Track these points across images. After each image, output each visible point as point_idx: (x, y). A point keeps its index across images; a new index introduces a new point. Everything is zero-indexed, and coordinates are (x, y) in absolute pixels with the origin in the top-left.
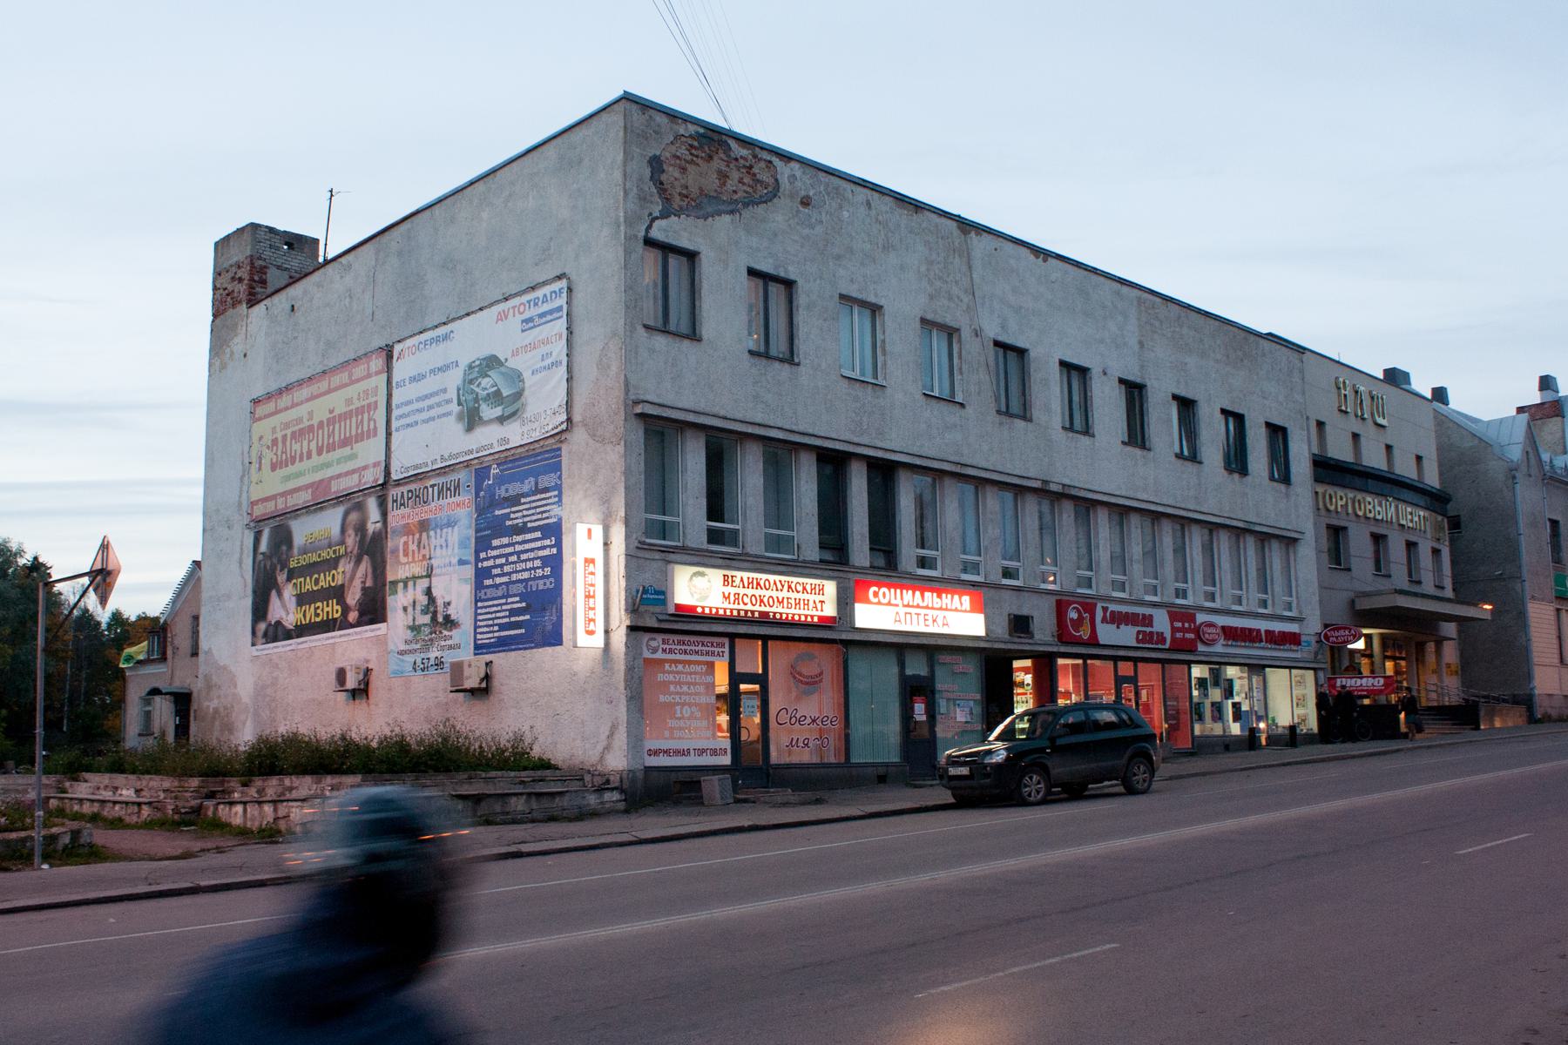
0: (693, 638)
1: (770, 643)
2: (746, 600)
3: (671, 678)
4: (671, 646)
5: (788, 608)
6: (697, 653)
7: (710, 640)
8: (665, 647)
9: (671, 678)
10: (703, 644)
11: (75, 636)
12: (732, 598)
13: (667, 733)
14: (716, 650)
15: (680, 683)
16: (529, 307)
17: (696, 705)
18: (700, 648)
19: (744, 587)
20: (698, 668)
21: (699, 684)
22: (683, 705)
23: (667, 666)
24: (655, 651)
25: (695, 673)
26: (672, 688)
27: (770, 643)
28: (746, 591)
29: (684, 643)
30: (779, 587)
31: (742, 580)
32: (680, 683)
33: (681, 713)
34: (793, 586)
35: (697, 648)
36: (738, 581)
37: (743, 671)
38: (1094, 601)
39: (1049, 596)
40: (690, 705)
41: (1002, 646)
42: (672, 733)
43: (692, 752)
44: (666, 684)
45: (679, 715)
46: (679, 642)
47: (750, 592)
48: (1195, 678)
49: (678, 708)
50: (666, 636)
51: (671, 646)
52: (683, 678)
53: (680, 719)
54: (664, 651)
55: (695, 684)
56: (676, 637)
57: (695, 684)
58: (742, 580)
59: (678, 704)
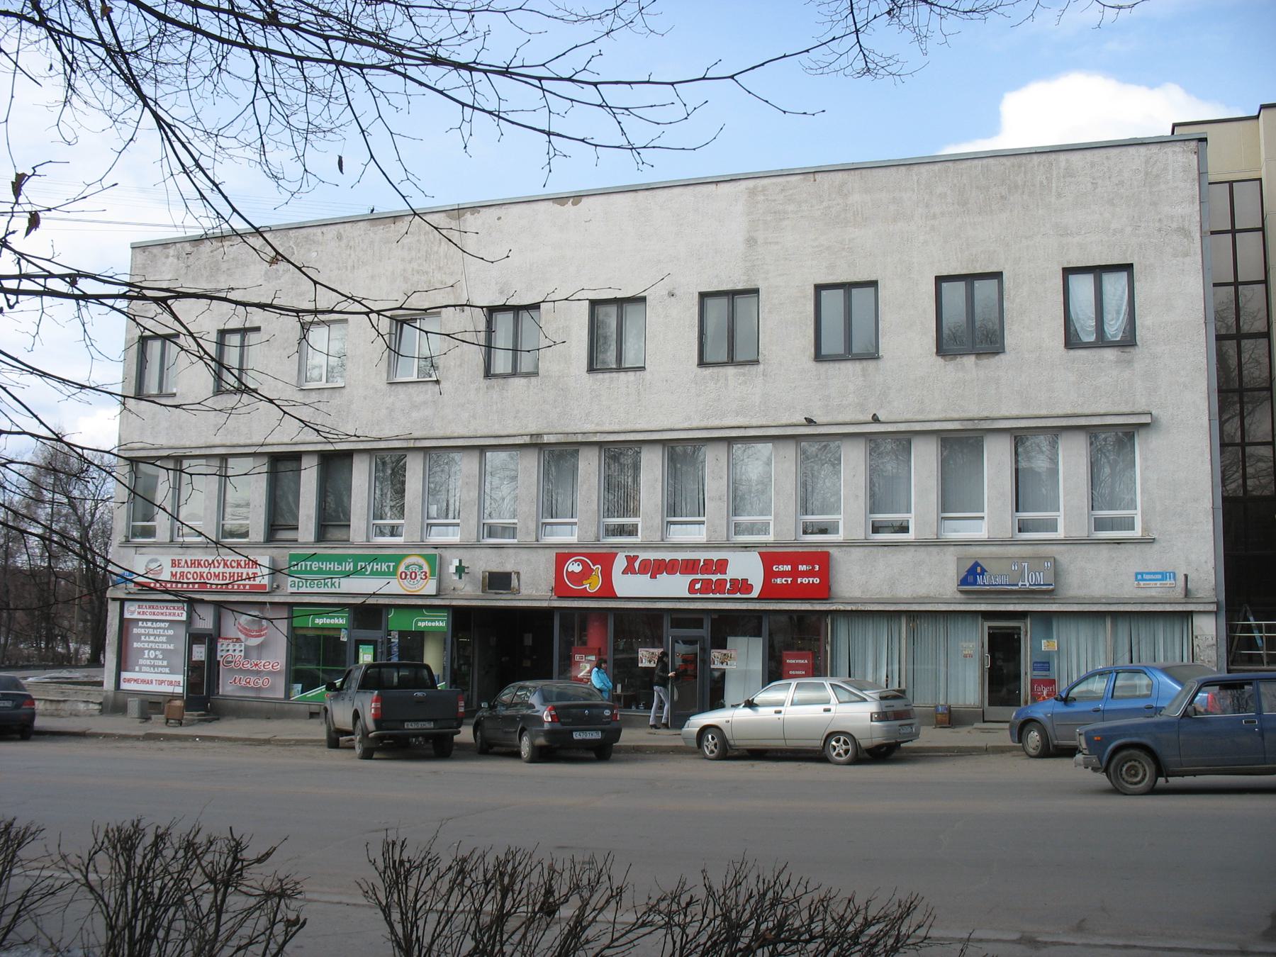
0: (159, 604)
1: (1261, 233)
2: (189, 576)
3: (143, 631)
4: (182, 570)
5: (223, 580)
6: (162, 614)
7: (235, 559)
8: (174, 570)
9: (143, 631)
10: (225, 564)
11: (365, 685)
12: (178, 575)
13: (137, 669)
14: (177, 612)
15: (149, 635)
16: (160, 838)
17: (159, 650)
18: (165, 610)
19: (188, 567)
20: (162, 625)
21: (163, 636)
22: (151, 649)
23: (140, 623)
24: (133, 613)
25: (160, 628)
26: (143, 638)
27: (1261, 233)
28: (189, 570)
29: (199, 564)
30: (216, 564)
31: (186, 562)
32: (149, 635)
33: (148, 655)
34: (228, 563)
35: (162, 611)
36: (183, 563)
37: (211, 624)
38: (614, 550)
39: (548, 551)
40: (155, 650)
41: (545, 604)
42: (140, 669)
43: (154, 682)
44: (139, 635)
45: (146, 656)
46: (150, 607)
47: (192, 570)
48: (1229, 671)
49: (146, 652)
50: (141, 603)
51: (182, 570)
52: (151, 631)
53: (146, 659)
54: (139, 613)
55: (159, 636)
56: (148, 604)
57: (159, 636)
58: (186, 562)
59: (146, 649)
